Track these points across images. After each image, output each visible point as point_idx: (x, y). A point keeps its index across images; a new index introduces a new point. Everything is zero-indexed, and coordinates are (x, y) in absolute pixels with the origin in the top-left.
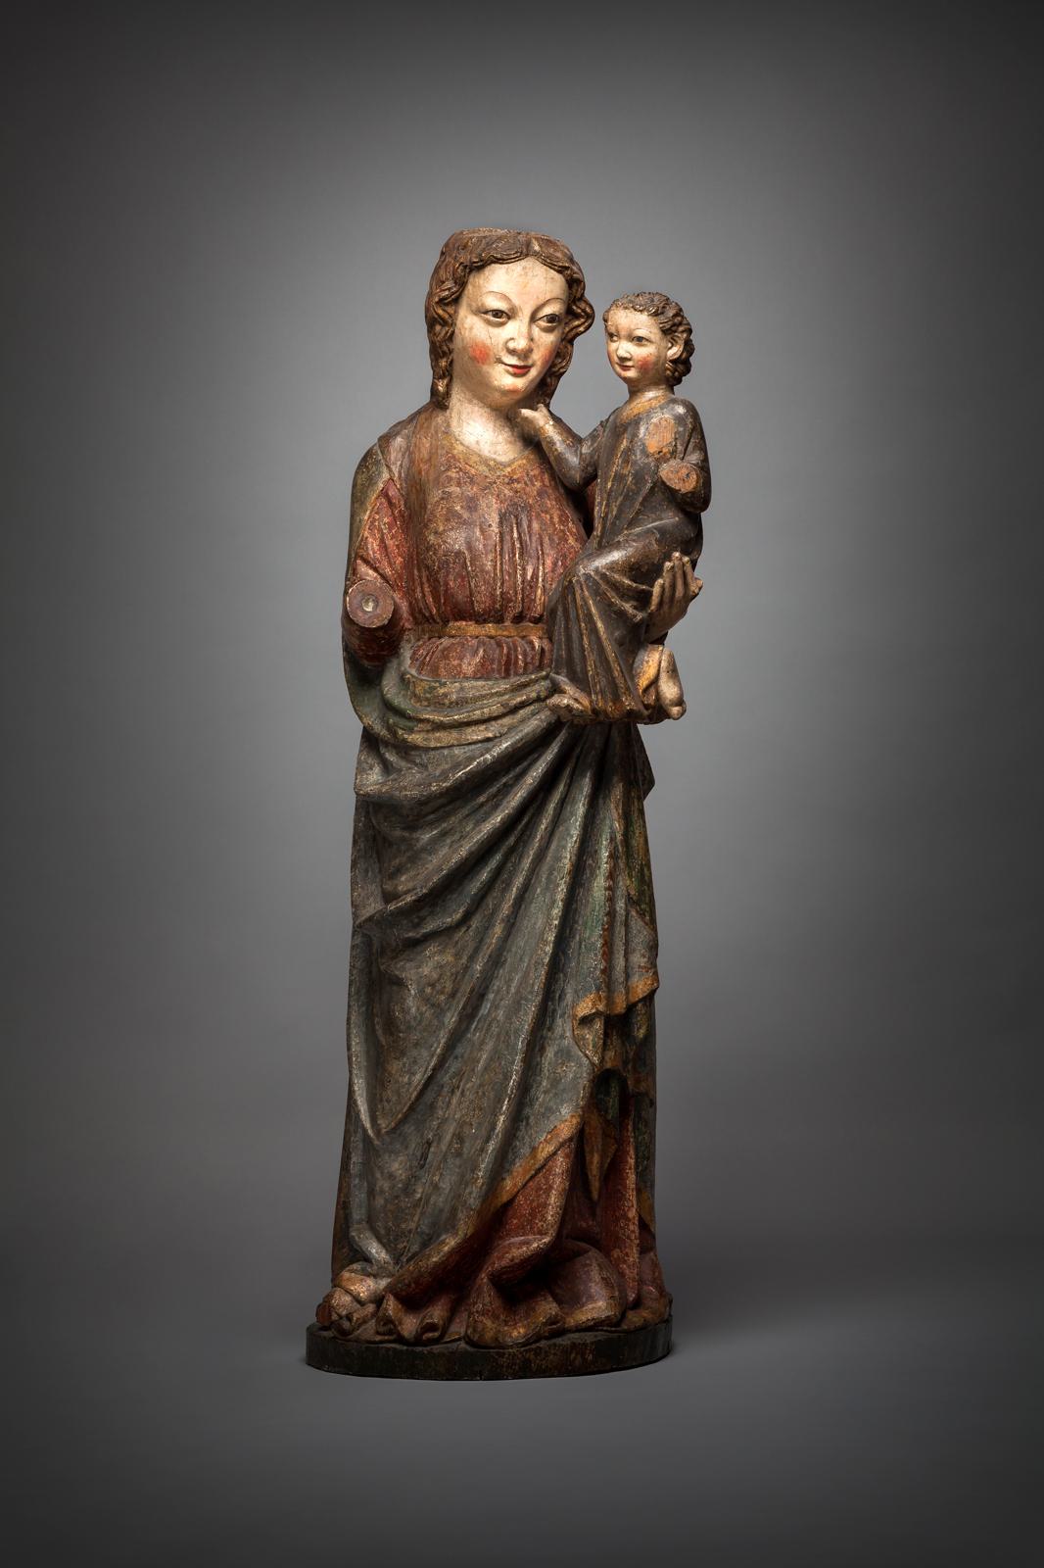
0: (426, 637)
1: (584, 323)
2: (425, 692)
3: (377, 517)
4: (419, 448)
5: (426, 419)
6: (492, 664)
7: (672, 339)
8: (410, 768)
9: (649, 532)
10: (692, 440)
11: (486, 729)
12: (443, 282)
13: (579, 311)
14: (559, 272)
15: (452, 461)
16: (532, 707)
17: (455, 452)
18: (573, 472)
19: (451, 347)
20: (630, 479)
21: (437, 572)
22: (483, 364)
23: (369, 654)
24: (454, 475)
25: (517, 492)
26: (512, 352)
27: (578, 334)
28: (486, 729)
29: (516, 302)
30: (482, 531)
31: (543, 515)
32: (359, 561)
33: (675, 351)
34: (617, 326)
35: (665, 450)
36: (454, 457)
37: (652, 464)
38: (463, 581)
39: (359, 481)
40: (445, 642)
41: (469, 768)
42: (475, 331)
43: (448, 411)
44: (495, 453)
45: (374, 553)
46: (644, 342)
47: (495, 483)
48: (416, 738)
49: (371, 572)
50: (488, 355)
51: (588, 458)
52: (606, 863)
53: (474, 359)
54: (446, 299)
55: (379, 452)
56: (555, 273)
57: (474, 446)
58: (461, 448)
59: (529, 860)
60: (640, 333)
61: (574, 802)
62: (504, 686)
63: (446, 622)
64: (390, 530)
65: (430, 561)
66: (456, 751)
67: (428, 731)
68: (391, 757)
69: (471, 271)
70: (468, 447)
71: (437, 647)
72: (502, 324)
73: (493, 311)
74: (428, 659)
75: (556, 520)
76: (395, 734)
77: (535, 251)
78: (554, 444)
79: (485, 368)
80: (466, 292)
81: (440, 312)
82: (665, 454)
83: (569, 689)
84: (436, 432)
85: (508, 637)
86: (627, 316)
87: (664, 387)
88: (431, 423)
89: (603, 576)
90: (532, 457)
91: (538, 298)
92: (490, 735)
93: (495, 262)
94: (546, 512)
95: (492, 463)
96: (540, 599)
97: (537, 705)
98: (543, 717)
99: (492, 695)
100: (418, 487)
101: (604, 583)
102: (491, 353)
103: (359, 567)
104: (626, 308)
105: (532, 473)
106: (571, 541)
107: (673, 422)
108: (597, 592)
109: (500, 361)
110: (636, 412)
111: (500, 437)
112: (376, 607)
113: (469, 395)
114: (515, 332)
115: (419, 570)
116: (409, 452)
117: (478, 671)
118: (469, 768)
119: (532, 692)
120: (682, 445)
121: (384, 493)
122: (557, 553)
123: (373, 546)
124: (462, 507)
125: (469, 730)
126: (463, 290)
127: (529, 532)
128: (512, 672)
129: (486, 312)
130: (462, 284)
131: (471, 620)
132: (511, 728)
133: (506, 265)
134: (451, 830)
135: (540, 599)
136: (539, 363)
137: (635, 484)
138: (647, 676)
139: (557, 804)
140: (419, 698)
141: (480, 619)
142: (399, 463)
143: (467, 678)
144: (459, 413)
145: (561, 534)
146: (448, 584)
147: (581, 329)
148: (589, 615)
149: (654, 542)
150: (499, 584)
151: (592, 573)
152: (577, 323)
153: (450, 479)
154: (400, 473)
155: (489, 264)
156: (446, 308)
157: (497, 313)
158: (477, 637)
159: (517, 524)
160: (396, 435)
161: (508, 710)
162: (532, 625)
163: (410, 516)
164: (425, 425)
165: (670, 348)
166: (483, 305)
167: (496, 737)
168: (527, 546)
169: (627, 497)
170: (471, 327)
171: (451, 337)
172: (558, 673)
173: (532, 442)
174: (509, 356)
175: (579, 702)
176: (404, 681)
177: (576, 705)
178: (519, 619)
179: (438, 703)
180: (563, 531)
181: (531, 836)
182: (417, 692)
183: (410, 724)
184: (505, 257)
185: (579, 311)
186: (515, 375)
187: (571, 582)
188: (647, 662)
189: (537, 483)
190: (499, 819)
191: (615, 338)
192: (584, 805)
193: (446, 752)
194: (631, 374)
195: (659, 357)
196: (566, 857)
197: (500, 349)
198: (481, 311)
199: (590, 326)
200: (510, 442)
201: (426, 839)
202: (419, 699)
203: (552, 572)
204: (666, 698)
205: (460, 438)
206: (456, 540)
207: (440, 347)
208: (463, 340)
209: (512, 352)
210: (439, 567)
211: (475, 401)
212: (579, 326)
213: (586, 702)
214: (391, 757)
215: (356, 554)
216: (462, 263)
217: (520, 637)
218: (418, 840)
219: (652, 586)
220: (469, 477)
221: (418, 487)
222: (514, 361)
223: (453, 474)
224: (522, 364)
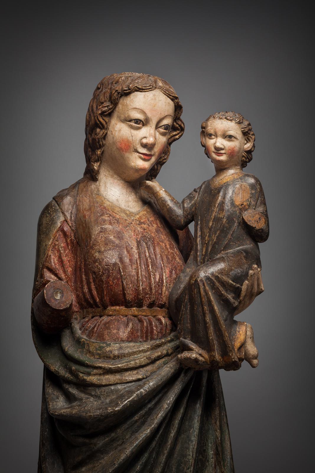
0: (90, 316)
1: (178, 134)
2: (97, 349)
3: (57, 243)
4: (82, 203)
5: (84, 187)
6: (137, 332)
7: (248, 138)
8: (88, 398)
9: (239, 252)
10: (260, 199)
11: (137, 373)
12: (102, 103)
13: (178, 126)
14: (172, 100)
15: (104, 210)
16: (164, 360)
17: (105, 205)
18: (180, 218)
19: (104, 142)
20: (225, 220)
21: (102, 276)
22: (126, 152)
23: (50, 328)
24: (107, 218)
25: (145, 229)
26: (145, 146)
27: (175, 140)
28: (137, 373)
29: (149, 115)
30: (128, 252)
31: (161, 243)
32: (45, 270)
33: (248, 146)
34: (215, 129)
35: (245, 204)
36: (105, 208)
37: (238, 212)
38: (118, 281)
39: (44, 222)
40: (105, 319)
41: (131, 398)
42: (122, 132)
43: (98, 182)
44: (128, 207)
45: (55, 264)
46: (233, 139)
47: (131, 223)
48: (93, 379)
49: (53, 276)
50: (129, 146)
51: (189, 210)
52: (212, 458)
53: (120, 149)
54: (105, 112)
55: (56, 205)
56: (170, 100)
57: (115, 203)
58: (108, 203)
59: (165, 457)
60: (231, 133)
61: (191, 419)
62: (146, 346)
63: (105, 307)
64: (65, 251)
65: (96, 269)
66: (119, 387)
67: (100, 375)
68: (73, 391)
69: (121, 97)
70: (112, 203)
71: (101, 322)
72: (139, 128)
73: (135, 120)
74: (95, 329)
75: (168, 247)
76: (77, 376)
77: (160, 86)
78: (166, 202)
79: (127, 155)
80: (117, 109)
81: (101, 120)
82: (245, 206)
83: (193, 346)
84: (92, 194)
85: (145, 316)
86: (222, 123)
87: (239, 167)
88: (88, 189)
89: (217, 278)
90: (149, 210)
91: (161, 114)
92: (140, 377)
93: (137, 91)
94: (162, 242)
95: (128, 212)
96: (165, 293)
97: (166, 358)
98: (172, 366)
99: (140, 352)
100: (84, 225)
101: (214, 282)
102: (132, 145)
103: (45, 274)
104: (221, 118)
105: (150, 219)
106: (177, 259)
107: (248, 187)
108: (213, 287)
109: (136, 151)
110: (225, 181)
111: (130, 198)
112: (62, 296)
113: (111, 172)
114: (147, 134)
115: (87, 275)
116: (76, 205)
117: (130, 336)
118: (131, 398)
119: (163, 350)
120: (254, 201)
121: (61, 229)
122: (172, 266)
123: (54, 261)
124: (114, 237)
125: (127, 374)
126: (115, 108)
127: (154, 253)
128: (149, 338)
129: (130, 121)
130: (115, 103)
131: (122, 305)
132: (153, 372)
133: (144, 93)
134: (117, 437)
135: (165, 293)
136: (157, 154)
137: (228, 223)
138: (239, 340)
139: (180, 420)
140: (93, 353)
141: (128, 304)
142: (70, 211)
143: (123, 341)
144: (105, 183)
145: (172, 255)
146: (109, 283)
147: (177, 137)
148: (209, 301)
149: (243, 258)
150: (141, 284)
151: (210, 276)
152: (175, 133)
153: (105, 221)
154: (71, 217)
155: (133, 92)
156: (104, 118)
157: (137, 121)
158: (126, 316)
159: (147, 248)
160: (67, 195)
161: (150, 361)
162: (159, 309)
163: (77, 243)
164: (84, 190)
165: (246, 144)
166: (129, 116)
167: (144, 378)
168: (154, 261)
169: (222, 231)
170: (119, 130)
171: (105, 137)
172: (185, 338)
173: (150, 202)
174: (142, 148)
175: (202, 356)
176: (78, 342)
177: (200, 358)
178: (151, 305)
179: (107, 357)
180: (173, 253)
181: (166, 441)
182: (91, 350)
183: (88, 370)
184: (144, 88)
185: (178, 126)
186: (144, 160)
187: (196, 281)
188: (239, 332)
189: (154, 227)
190: (149, 431)
191: (213, 137)
192: (198, 421)
193: (112, 388)
194: (223, 158)
195: (240, 148)
196: (189, 455)
197: (137, 144)
198: (128, 120)
199: (182, 135)
200: (136, 201)
201: (101, 444)
202: (92, 354)
203: (170, 277)
204: (250, 354)
205: (107, 197)
206: (111, 257)
207: (99, 142)
208: (113, 138)
209: (145, 146)
210: (103, 272)
211: (115, 176)
212: (176, 135)
213: (206, 356)
214: (73, 391)
215: (43, 265)
216: (117, 91)
217: (152, 316)
218: (95, 445)
219: (242, 285)
220: (116, 220)
221: (84, 225)
222: (144, 151)
223: (106, 217)
224: (149, 153)
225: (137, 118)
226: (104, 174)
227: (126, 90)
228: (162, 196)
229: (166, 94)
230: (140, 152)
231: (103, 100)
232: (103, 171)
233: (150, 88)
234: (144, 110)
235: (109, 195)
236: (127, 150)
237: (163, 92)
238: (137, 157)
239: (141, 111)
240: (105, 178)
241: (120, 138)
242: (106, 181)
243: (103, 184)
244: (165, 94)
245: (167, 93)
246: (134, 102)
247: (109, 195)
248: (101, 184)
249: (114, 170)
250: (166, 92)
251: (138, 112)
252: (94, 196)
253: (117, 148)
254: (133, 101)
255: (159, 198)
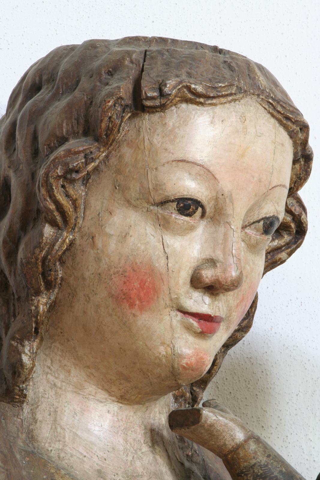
29: (226, 184)
225: (185, 194)
226: (48, 381)
227: (153, 98)
228: (253, 462)
229: (275, 113)
230: (189, 308)
231: (64, 130)
232: (47, 370)
233: (231, 94)
234: (211, 169)
235: (72, 456)
236: (148, 302)
237: (267, 107)
238: (179, 325)
239: (202, 172)
240: (52, 393)
241: (123, 261)
242: (56, 404)
243: (46, 414)
244: (273, 116)
245: (279, 112)
246: (178, 140)
247: (72, 456)
248: (39, 417)
249: (88, 367)
250: (275, 108)
251: (190, 174)
252: (18, 457)
253: (111, 295)
254: (175, 137)
255: (245, 467)
